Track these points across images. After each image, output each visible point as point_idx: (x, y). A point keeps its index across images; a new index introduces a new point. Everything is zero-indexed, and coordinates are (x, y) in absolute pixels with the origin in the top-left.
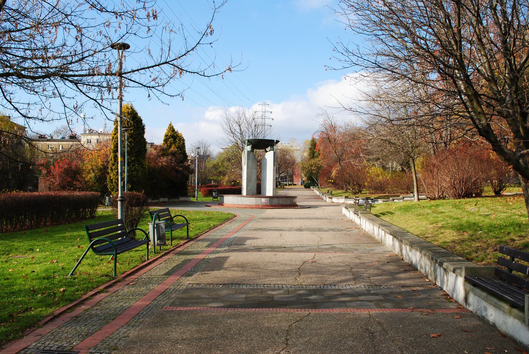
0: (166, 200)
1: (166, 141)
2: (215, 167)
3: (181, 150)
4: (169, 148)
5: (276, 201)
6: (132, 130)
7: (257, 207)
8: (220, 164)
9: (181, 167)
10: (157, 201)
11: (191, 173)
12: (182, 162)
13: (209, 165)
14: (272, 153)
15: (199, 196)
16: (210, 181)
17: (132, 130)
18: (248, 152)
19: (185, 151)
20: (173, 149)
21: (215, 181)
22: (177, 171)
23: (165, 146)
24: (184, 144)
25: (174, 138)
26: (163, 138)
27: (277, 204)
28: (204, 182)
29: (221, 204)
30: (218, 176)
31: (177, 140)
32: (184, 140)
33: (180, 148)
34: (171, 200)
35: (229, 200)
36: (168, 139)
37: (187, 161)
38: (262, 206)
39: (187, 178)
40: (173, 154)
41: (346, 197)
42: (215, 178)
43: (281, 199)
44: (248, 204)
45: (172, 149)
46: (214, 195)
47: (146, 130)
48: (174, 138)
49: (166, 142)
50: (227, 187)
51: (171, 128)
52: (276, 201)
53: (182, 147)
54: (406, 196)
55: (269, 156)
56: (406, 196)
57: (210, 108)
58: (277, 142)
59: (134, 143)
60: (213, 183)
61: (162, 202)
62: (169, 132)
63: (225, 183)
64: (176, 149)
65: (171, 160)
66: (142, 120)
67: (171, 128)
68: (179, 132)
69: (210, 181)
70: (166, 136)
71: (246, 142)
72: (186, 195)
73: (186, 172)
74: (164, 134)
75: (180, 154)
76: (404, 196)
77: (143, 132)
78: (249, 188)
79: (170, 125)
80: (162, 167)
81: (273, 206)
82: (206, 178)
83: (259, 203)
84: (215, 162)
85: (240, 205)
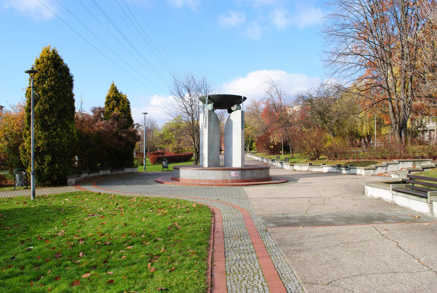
0: (108, 172)
1: (107, 103)
2: (162, 136)
3: (125, 113)
4: (112, 112)
5: (249, 175)
6: (53, 80)
7: (224, 183)
8: (165, 134)
9: (125, 133)
10: (97, 174)
11: (137, 141)
12: (127, 127)
13: (156, 135)
14: (239, 112)
15: (147, 166)
16: (156, 149)
17: (53, 80)
18: (209, 111)
19: (130, 115)
20: (116, 112)
21: (160, 148)
22: (121, 138)
23: (107, 109)
24: (129, 107)
25: (117, 102)
26: (104, 100)
27: (250, 178)
28: (151, 150)
29: (176, 179)
30: (164, 144)
31: (121, 102)
32: (128, 103)
33: (124, 111)
34: (115, 172)
35: (187, 173)
36: (110, 101)
37: (133, 126)
38: (233, 181)
39: (133, 147)
40: (116, 118)
41: (310, 164)
42: (162, 146)
43: (255, 171)
44: (213, 179)
45: (115, 112)
46: (164, 164)
47: (75, 83)
48: (117, 102)
49: (108, 105)
50: (173, 154)
51: (114, 90)
52: (249, 175)
53: (127, 111)
54: (391, 162)
55: (236, 117)
56: (391, 162)
57: (155, 96)
58: (245, 98)
59: (55, 99)
60: (159, 151)
61: (103, 176)
62: (111, 93)
63: (171, 151)
64: (120, 113)
65: (113, 124)
66: (68, 70)
67: (114, 90)
68: (123, 94)
69: (156, 149)
70: (108, 97)
71: (207, 98)
72: (132, 166)
73: (131, 139)
74: (105, 96)
75: (124, 118)
76: (388, 163)
77: (71, 85)
78: (211, 157)
79: (113, 85)
80: (99, 133)
81: (246, 181)
82: (154, 146)
83: (228, 177)
84: (161, 132)
85: (201, 181)
